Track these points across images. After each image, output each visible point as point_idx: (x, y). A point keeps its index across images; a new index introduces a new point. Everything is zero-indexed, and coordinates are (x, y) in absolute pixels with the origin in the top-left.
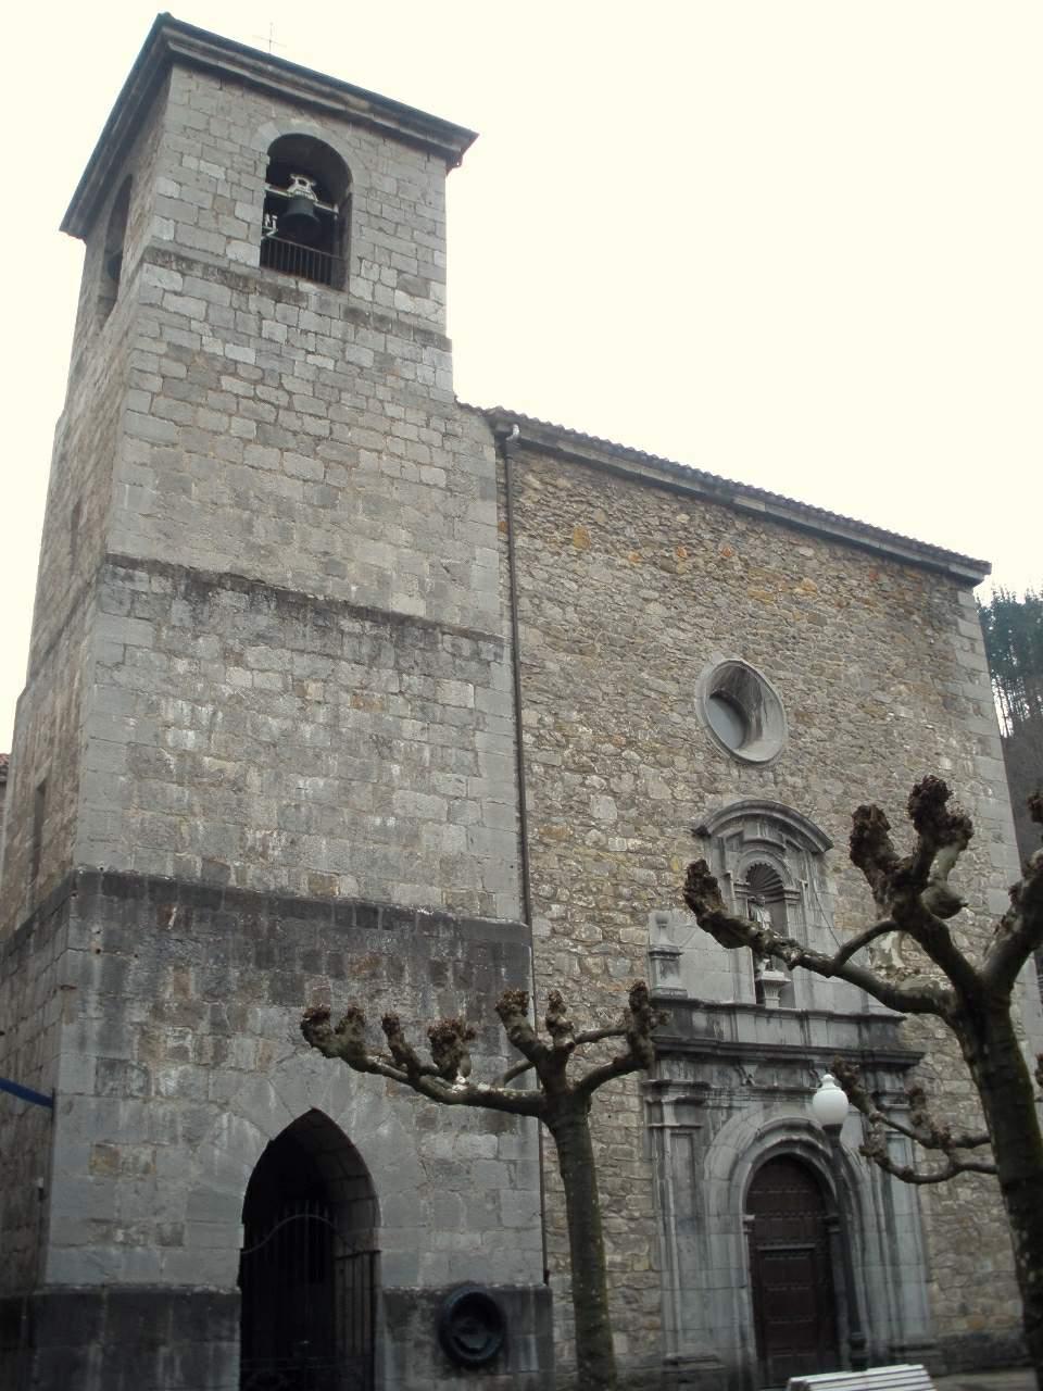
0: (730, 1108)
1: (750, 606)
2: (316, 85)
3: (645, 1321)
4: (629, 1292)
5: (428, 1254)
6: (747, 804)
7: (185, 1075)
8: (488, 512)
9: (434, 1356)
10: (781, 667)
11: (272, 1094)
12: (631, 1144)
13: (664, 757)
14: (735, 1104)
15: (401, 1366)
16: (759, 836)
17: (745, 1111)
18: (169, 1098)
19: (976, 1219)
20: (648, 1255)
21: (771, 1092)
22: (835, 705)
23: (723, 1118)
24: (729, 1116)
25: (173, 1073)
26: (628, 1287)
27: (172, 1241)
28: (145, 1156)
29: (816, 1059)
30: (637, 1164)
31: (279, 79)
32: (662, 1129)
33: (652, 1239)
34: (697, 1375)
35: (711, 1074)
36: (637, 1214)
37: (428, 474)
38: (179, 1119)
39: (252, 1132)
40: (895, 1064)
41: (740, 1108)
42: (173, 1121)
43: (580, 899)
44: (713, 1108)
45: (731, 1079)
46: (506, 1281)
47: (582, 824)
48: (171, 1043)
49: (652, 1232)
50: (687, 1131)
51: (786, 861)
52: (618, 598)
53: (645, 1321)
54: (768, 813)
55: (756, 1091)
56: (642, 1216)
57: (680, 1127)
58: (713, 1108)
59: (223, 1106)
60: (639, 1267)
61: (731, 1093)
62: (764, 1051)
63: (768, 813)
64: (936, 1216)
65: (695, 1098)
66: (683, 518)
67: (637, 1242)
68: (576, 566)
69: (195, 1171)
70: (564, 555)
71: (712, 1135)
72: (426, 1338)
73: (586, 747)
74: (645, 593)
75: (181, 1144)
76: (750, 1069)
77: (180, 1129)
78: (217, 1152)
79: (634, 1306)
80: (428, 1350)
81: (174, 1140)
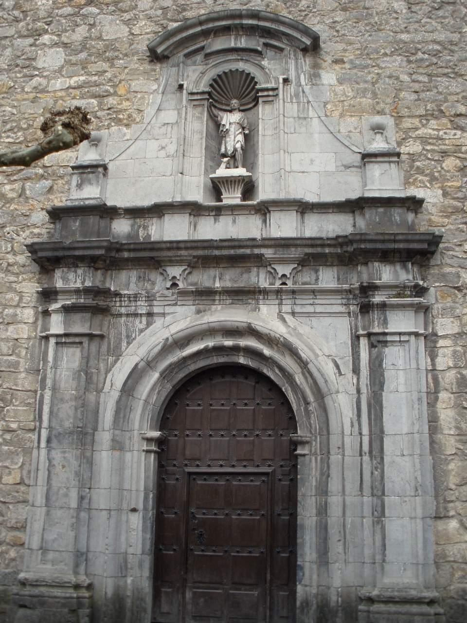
0: (150, 315)
3: (9, 536)
6: (215, 15)
12: (19, 356)
14: (156, 310)
16: (233, 45)
17: (168, 318)
20: (21, 467)
24: (149, 324)
29: (268, 253)
30: (23, 375)
32: (47, 338)
33: (28, 452)
34: (41, 601)
35: (127, 282)
36: (14, 426)
40: (394, 251)
41: (164, 315)
43: (8, 137)
44: (128, 315)
45: (154, 284)
47: (25, 76)
49: (28, 445)
50: (77, 340)
51: (265, 63)
54: (237, 22)
55: (183, 293)
56: (20, 428)
57: (66, 335)
58: (128, 315)
61: (150, 298)
62: (186, 248)
63: (237, 22)
65: (97, 304)
71: (124, 344)
76: (175, 271)
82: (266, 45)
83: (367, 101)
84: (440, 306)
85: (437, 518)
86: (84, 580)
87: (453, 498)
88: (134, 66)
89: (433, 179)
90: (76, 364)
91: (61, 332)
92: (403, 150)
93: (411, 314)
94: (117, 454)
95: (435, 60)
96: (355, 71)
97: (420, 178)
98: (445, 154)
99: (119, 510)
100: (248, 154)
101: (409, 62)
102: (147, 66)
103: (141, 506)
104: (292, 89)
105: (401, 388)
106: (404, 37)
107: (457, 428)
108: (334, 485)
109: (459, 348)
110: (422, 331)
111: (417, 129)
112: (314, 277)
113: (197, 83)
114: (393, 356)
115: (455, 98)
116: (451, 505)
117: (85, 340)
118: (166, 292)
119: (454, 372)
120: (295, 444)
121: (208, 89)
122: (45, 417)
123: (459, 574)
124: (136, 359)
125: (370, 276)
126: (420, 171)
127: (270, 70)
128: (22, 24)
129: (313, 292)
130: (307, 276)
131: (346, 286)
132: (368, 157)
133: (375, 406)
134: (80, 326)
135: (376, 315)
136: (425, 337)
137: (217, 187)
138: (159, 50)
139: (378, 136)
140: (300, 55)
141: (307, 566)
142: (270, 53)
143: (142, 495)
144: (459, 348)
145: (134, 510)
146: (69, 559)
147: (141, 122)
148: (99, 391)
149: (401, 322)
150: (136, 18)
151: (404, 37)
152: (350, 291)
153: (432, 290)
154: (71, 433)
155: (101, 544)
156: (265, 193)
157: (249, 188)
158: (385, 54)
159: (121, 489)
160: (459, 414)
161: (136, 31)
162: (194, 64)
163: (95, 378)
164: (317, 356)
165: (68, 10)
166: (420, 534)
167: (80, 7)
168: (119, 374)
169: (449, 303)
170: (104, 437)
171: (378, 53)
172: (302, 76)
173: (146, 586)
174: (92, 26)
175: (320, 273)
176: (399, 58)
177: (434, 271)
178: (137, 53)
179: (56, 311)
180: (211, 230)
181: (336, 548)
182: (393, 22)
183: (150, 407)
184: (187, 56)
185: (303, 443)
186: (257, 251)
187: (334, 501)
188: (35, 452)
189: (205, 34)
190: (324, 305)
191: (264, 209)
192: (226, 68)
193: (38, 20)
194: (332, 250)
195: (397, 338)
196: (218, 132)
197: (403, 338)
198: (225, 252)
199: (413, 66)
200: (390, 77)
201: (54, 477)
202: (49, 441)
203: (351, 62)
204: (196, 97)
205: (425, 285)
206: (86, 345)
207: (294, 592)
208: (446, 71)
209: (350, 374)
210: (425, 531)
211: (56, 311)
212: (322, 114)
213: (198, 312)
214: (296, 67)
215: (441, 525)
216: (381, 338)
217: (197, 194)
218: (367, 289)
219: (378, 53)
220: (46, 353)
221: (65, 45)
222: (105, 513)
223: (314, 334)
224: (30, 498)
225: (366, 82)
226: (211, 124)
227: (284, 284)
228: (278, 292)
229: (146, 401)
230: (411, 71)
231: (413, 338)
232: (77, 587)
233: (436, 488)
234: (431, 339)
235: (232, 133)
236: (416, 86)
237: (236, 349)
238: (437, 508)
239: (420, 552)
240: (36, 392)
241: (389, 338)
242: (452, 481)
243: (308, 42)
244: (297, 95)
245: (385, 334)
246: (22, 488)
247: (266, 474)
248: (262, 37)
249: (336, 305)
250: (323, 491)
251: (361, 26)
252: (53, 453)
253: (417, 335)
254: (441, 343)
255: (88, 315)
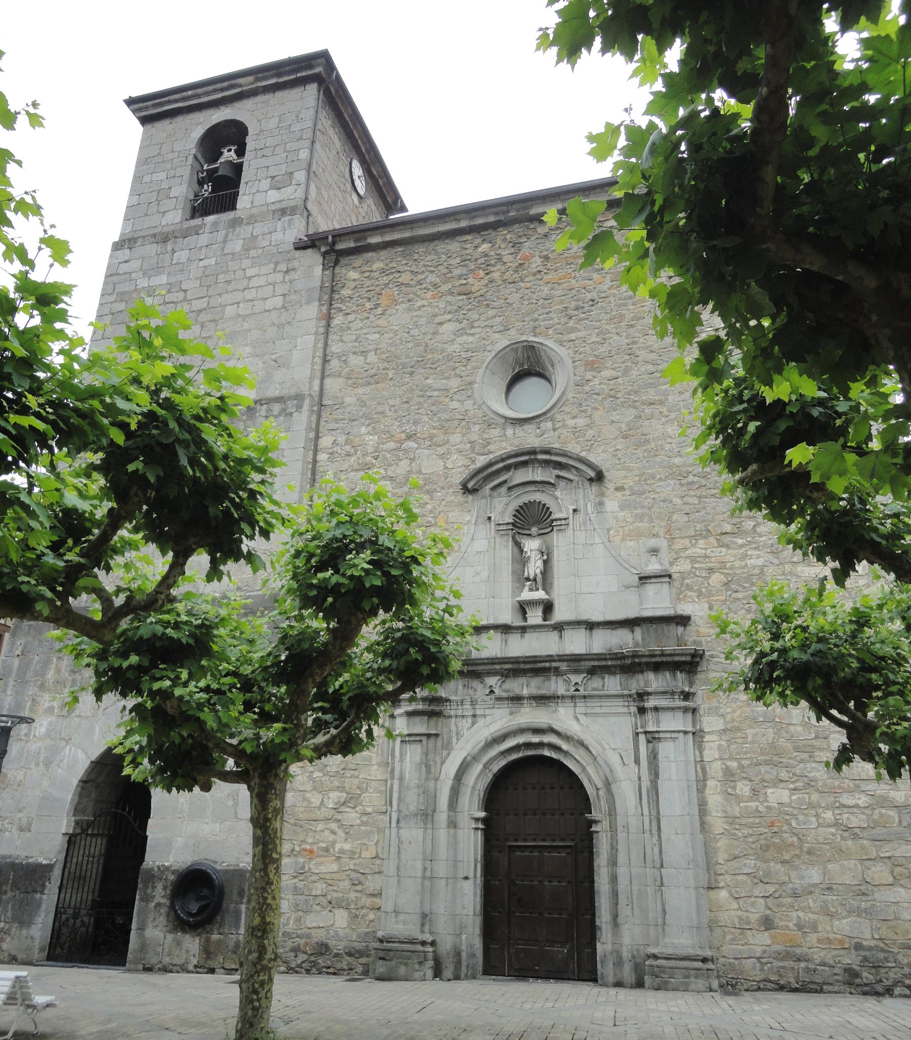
0: (474, 716)
1: (546, 290)
2: (219, 86)
3: (368, 902)
4: (354, 875)
5: (179, 839)
7: (50, 724)
8: (312, 311)
9: (168, 915)
10: (574, 330)
11: (97, 730)
13: (440, 438)
14: (478, 712)
15: (141, 929)
16: (530, 479)
17: (488, 719)
18: (40, 739)
19: (794, 824)
20: (376, 844)
21: (517, 699)
22: (634, 343)
23: (468, 725)
24: (473, 724)
25: (45, 723)
26: (355, 871)
27: (25, 829)
28: (20, 777)
29: (563, 666)
30: (375, 767)
31: (198, 96)
33: (380, 831)
36: (369, 810)
37: (269, 304)
38: (42, 751)
39: (81, 755)
42: (39, 753)
45: (476, 690)
46: (233, 861)
48: (47, 705)
50: (418, 738)
52: (415, 332)
53: (368, 902)
57: (409, 735)
59: (68, 741)
60: (367, 854)
62: (499, 663)
64: (731, 820)
66: (485, 247)
67: (368, 834)
68: (380, 322)
69: (45, 783)
70: (372, 316)
72: (163, 901)
73: (370, 449)
74: (438, 319)
75: (42, 767)
76: (492, 681)
77: (42, 758)
78: (60, 771)
79: (359, 888)
80: (164, 910)
81: (37, 764)
82: (558, 477)
83: (644, 525)
84: (706, 706)
85: (710, 888)
86: (429, 938)
87: (723, 871)
88: (449, 499)
89: (700, 594)
90: (417, 758)
91: (406, 732)
92: (673, 570)
93: (679, 715)
94: (452, 831)
95: (703, 482)
96: (634, 497)
97: (689, 593)
98: (711, 570)
99: (455, 878)
100: (545, 579)
101: (682, 485)
102: (460, 498)
103: (471, 875)
104: (580, 517)
105: (674, 777)
106: (677, 461)
107: (724, 811)
108: (622, 859)
109: (723, 743)
110: (690, 729)
111: (686, 549)
112: (601, 684)
113: (503, 513)
114: (666, 749)
115: (721, 517)
116: (721, 877)
117: (424, 739)
118: (486, 698)
119: (719, 762)
120: (591, 822)
121: (511, 521)
122: (395, 803)
123: (729, 937)
124: (464, 754)
125: (642, 683)
126: (689, 588)
127: (561, 502)
128: (353, 459)
129: (600, 697)
130: (596, 682)
131: (626, 692)
132: (644, 579)
133: (653, 792)
134: (421, 726)
135: (650, 716)
136: (694, 734)
137: (523, 608)
138: (470, 485)
139: (654, 558)
140: (587, 483)
141: (604, 927)
142: (562, 484)
143: (472, 865)
144: (723, 743)
145: (466, 878)
146: (417, 919)
147: (459, 550)
148: (436, 779)
149: (672, 722)
150: (449, 452)
151: (677, 461)
152: (630, 696)
153: (699, 693)
154: (416, 815)
155: (441, 908)
156: (559, 615)
157: (548, 608)
158: (661, 479)
159: (456, 861)
160: (726, 800)
161: (450, 465)
162: (499, 495)
163: (433, 770)
164: (605, 749)
165: (392, 445)
166: (694, 902)
167: (401, 442)
168: (451, 768)
169: (714, 703)
170: (442, 816)
171: (654, 478)
172: (589, 505)
173: (478, 944)
174: (413, 460)
175: (606, 680)
176: (672, 482)
177: (700, 676)
178: (451, 486)
179: (401, 715)
180: (520, 647)
181: (624, 911)
182: (667, 447)
183: (476, 793)
184: (494, 488)
185: (596, 822)
186: (554, 664)
187: (622, 871)
188: (387, 831)
189: (507, 468)
190: (609, 706)
191: (559, 627)
192: (526, 499)
193: (367, 454)
194: (614, 663)
195: (668, 735)
196: (521, 558)
197: (673, 735)
198: (528, 666)
199: (684, 488)
200: (664, 501)
201: (402, 851)
202: (398, 822)
203: (631, 488)
204: (502, 528)
205: (692, 690)
206: (424, 742)
207: (595, 949)
208: (713, 491)
209: (633, 765)
210: (698, 899)
211: (401, 715)
212: (606, 540)
213: (511, 714)
214: (586, 496)
215: (712, 893)
216: (657, 736)
217: (507, 617)
218: (641, 696)
219: (654, 478)
220: (393, 750)
221: (391, 479)
222: (443, 881)
223: (597, 735)
224: (383, 869)
225: (643, 507)
226: (516, 550)
227: (577, 690)
228: (573, 697)
229: (473, 788)
230: (682, 494)
231: (681, 735)
232: (423, 943)
233: (708, 863)
234: (697, 735)
235: (532, 559)
236: (687, 509)
237: (541, 745)
238: (709, 880)
239: (694, 917)
240: (386, 781)
241: (661, 735)
242: (721, 857)
243: (592, 474)
244: (585, 523)
245: (658, 732)
246: (378, 861)
247: (570, 847)
248: (555, 468)
249: (619, 706)
250: (613, 862)
251: (639, 452)
252: (402, 831)
253: (685, 733)
254: (707, 738)
255: (426, 718)
